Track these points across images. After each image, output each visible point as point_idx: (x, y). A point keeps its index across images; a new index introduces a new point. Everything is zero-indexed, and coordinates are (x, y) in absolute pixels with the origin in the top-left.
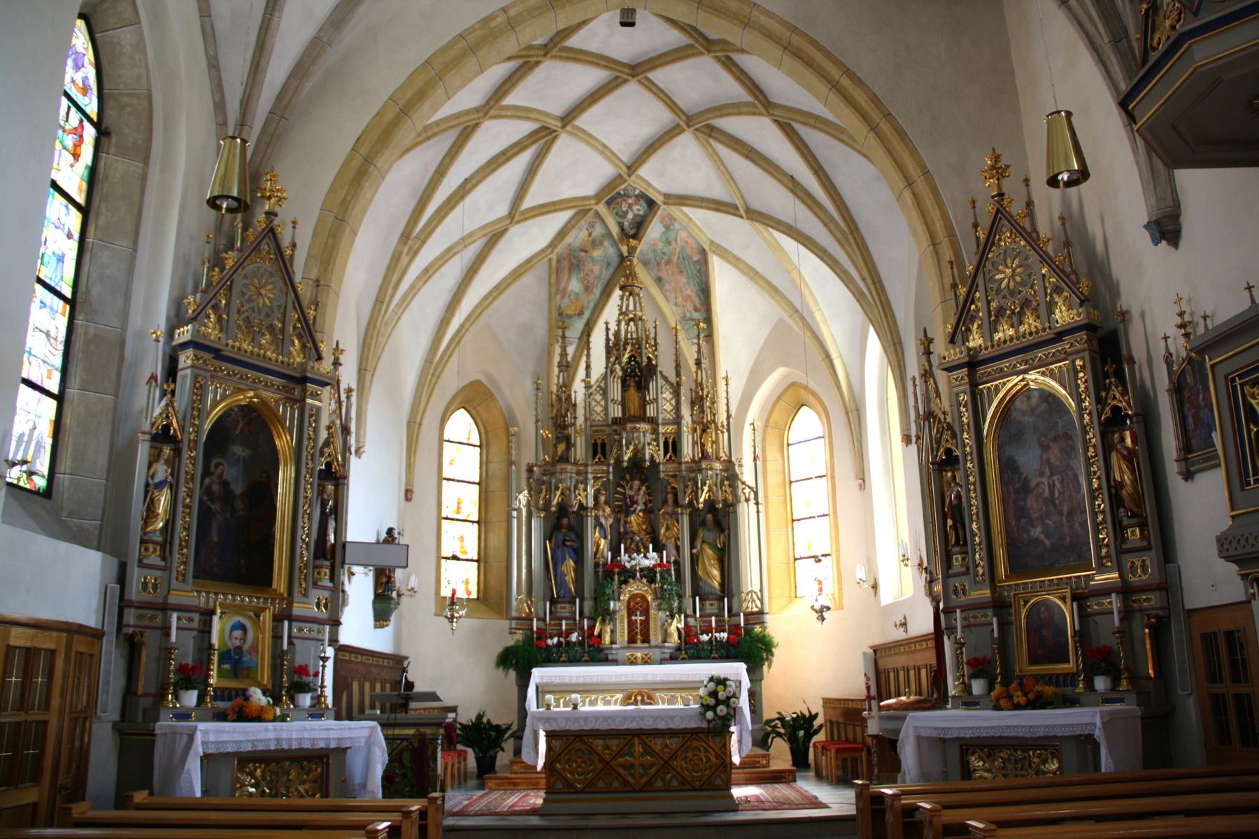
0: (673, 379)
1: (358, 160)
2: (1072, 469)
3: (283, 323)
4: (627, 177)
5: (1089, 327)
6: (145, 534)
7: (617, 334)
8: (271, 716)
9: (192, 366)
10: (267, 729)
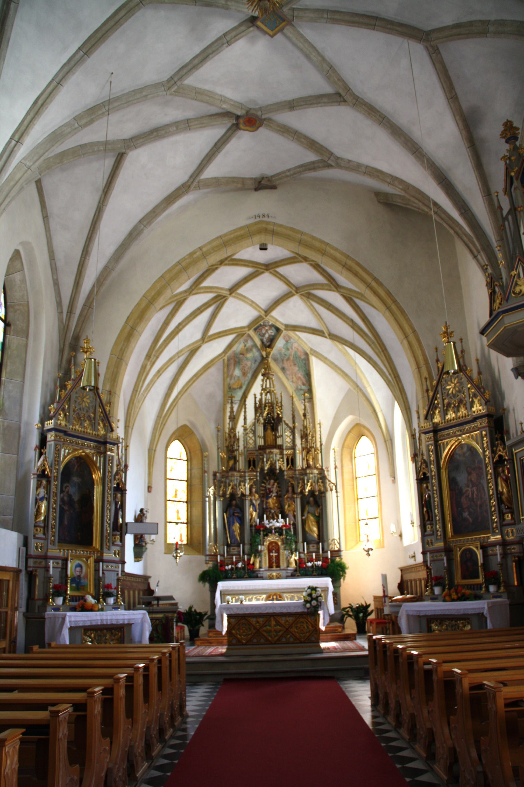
0: (291, 425)
1: (128, 328)
3: (95, 414)
4: (264, 317)
5: (488, 415)
6: (36, 523)
7: (261, 400)
8: (97, 609)
9: (54, 440)
10: (96, 615)
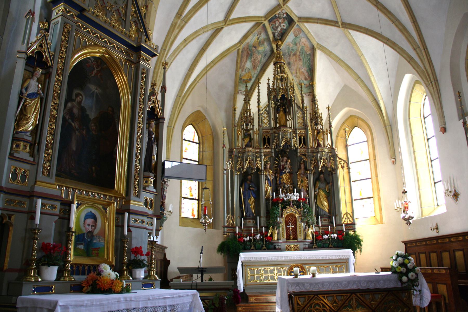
4: (282, 5)
8: (119, 289)
10: (119, 301)
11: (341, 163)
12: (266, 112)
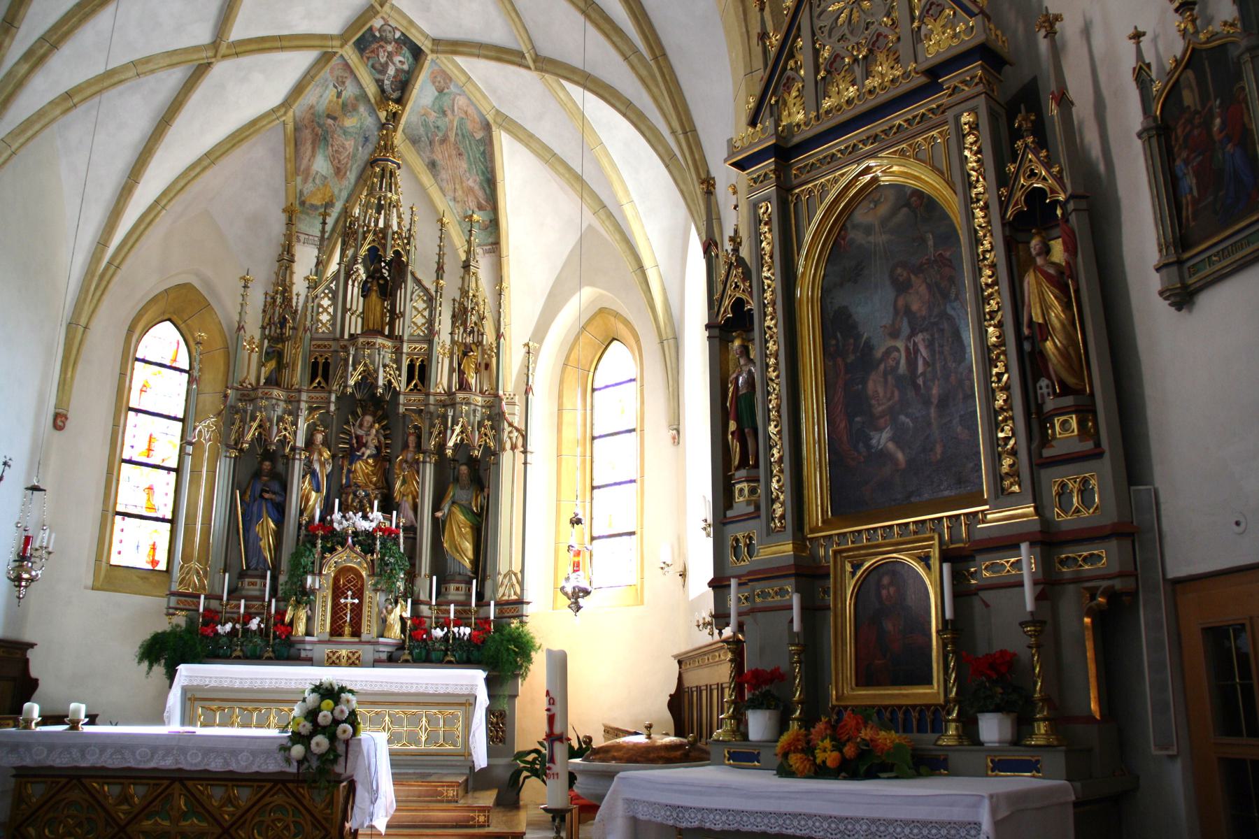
2: (950, 319)
4: (378, 8)
5: (986, 54)
11: (511, 435)
12: (329, 292)
